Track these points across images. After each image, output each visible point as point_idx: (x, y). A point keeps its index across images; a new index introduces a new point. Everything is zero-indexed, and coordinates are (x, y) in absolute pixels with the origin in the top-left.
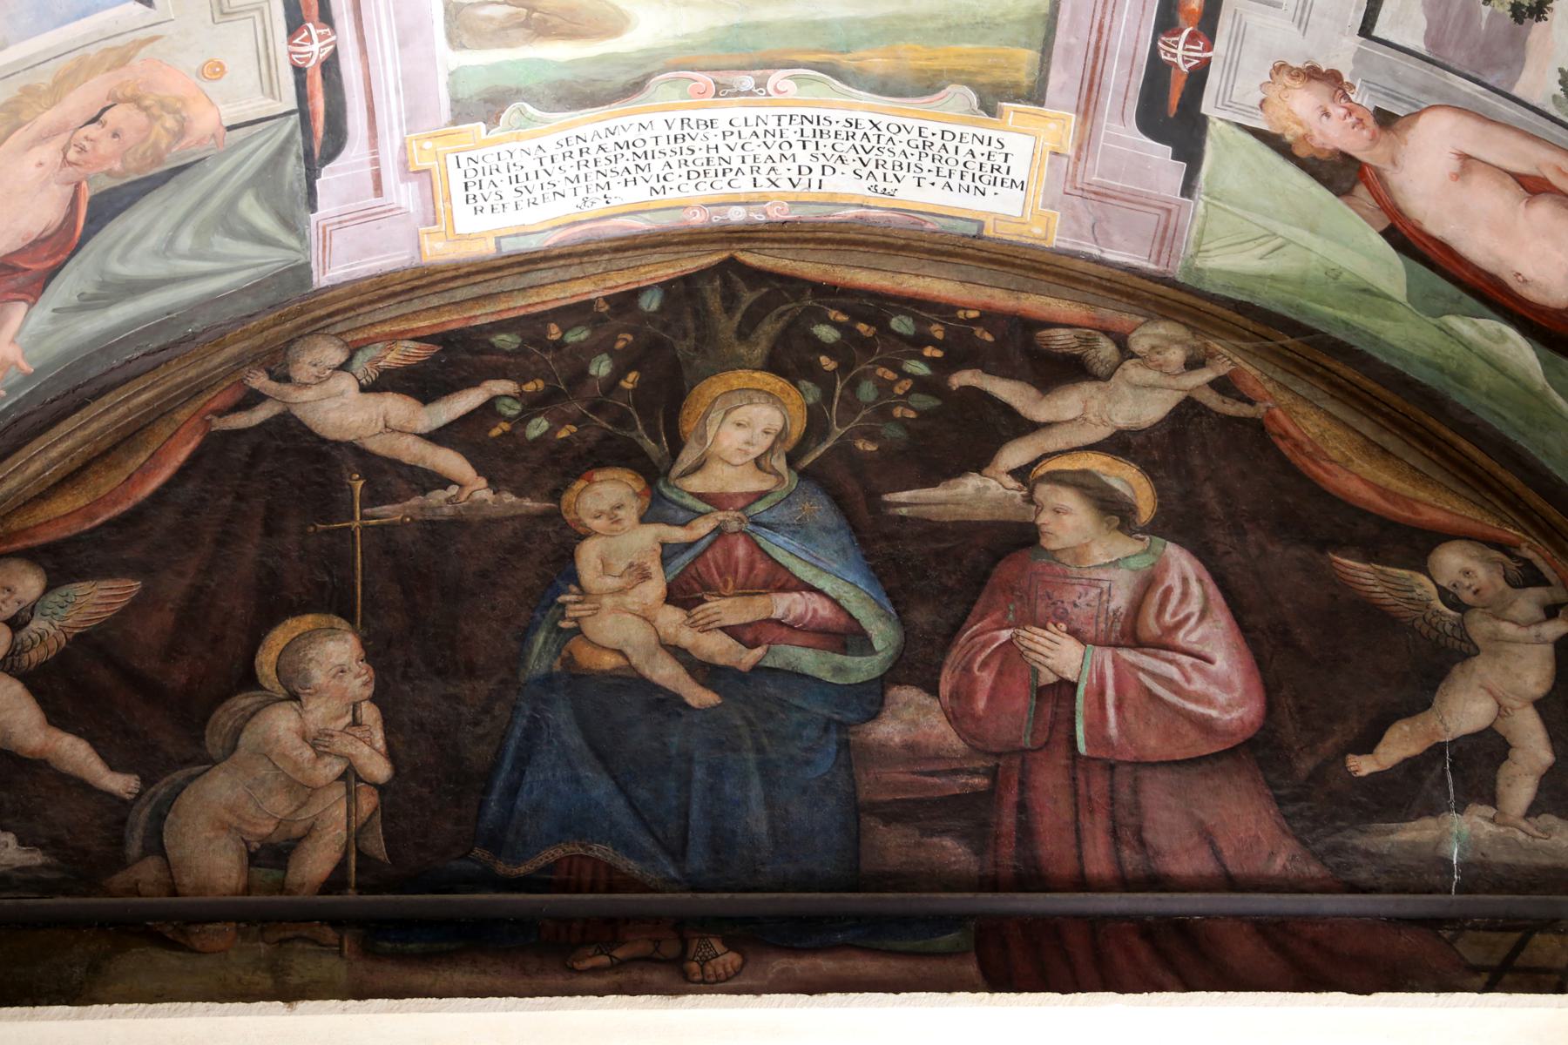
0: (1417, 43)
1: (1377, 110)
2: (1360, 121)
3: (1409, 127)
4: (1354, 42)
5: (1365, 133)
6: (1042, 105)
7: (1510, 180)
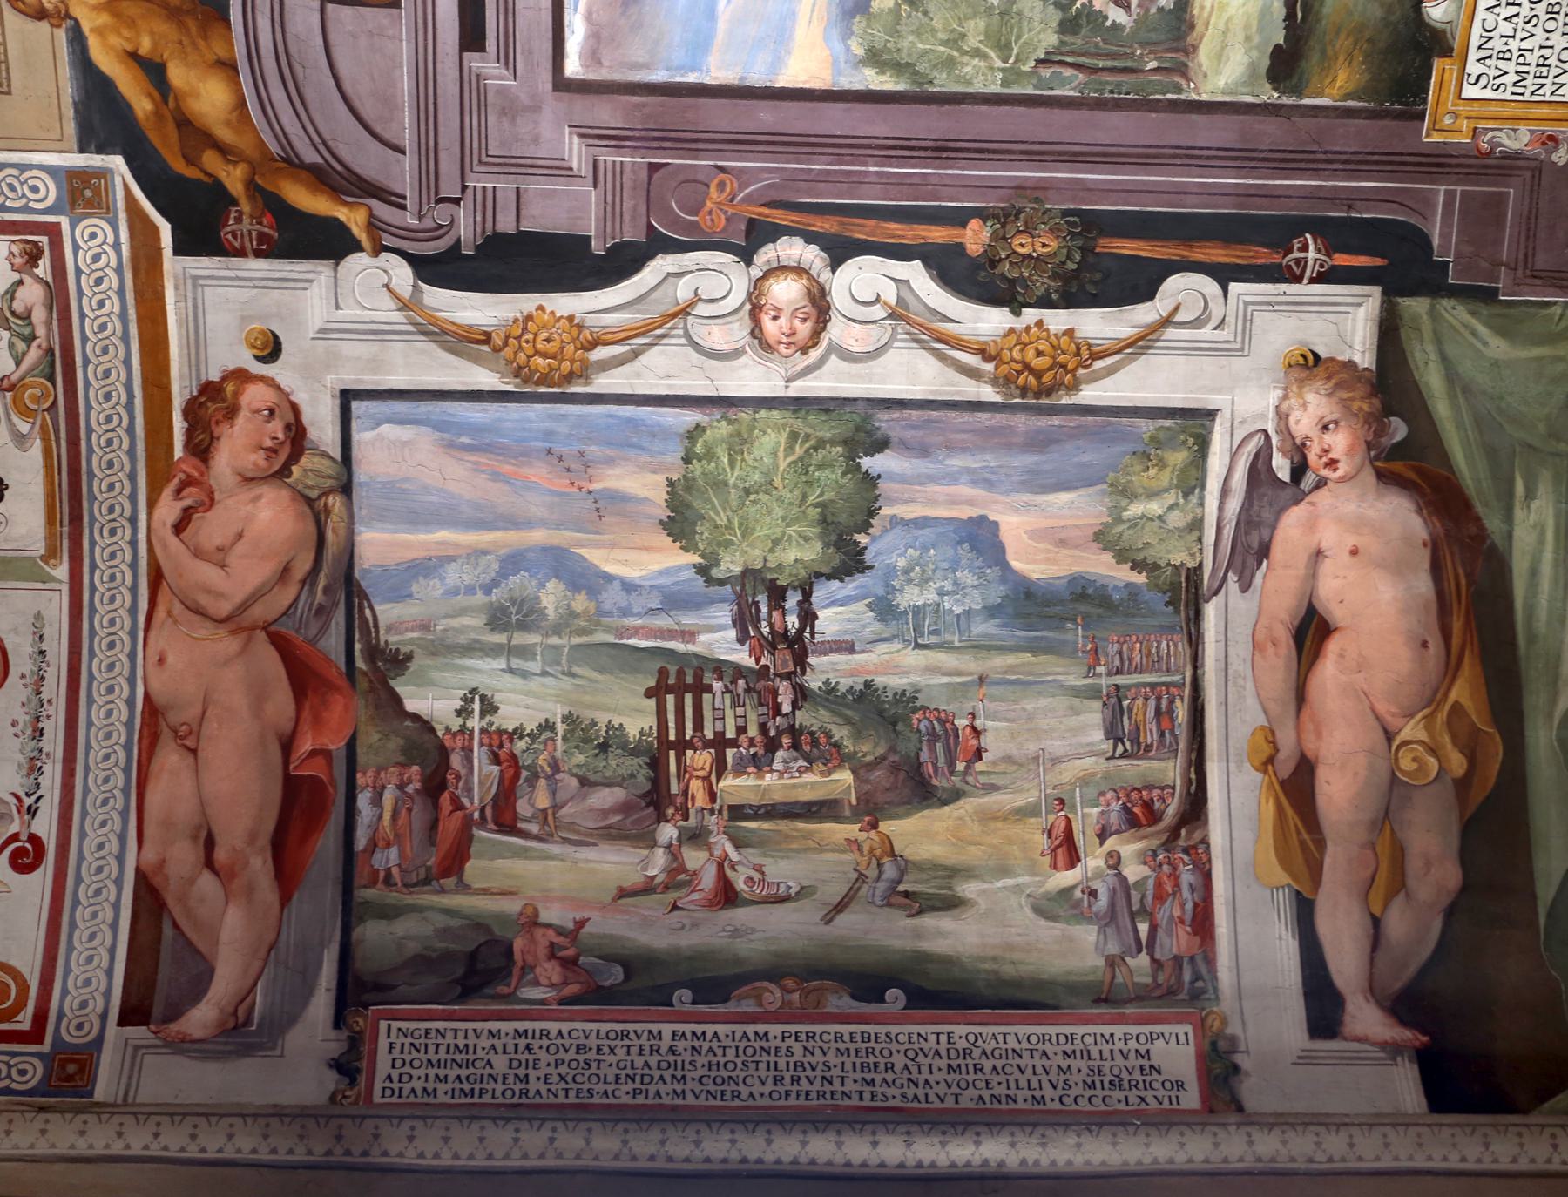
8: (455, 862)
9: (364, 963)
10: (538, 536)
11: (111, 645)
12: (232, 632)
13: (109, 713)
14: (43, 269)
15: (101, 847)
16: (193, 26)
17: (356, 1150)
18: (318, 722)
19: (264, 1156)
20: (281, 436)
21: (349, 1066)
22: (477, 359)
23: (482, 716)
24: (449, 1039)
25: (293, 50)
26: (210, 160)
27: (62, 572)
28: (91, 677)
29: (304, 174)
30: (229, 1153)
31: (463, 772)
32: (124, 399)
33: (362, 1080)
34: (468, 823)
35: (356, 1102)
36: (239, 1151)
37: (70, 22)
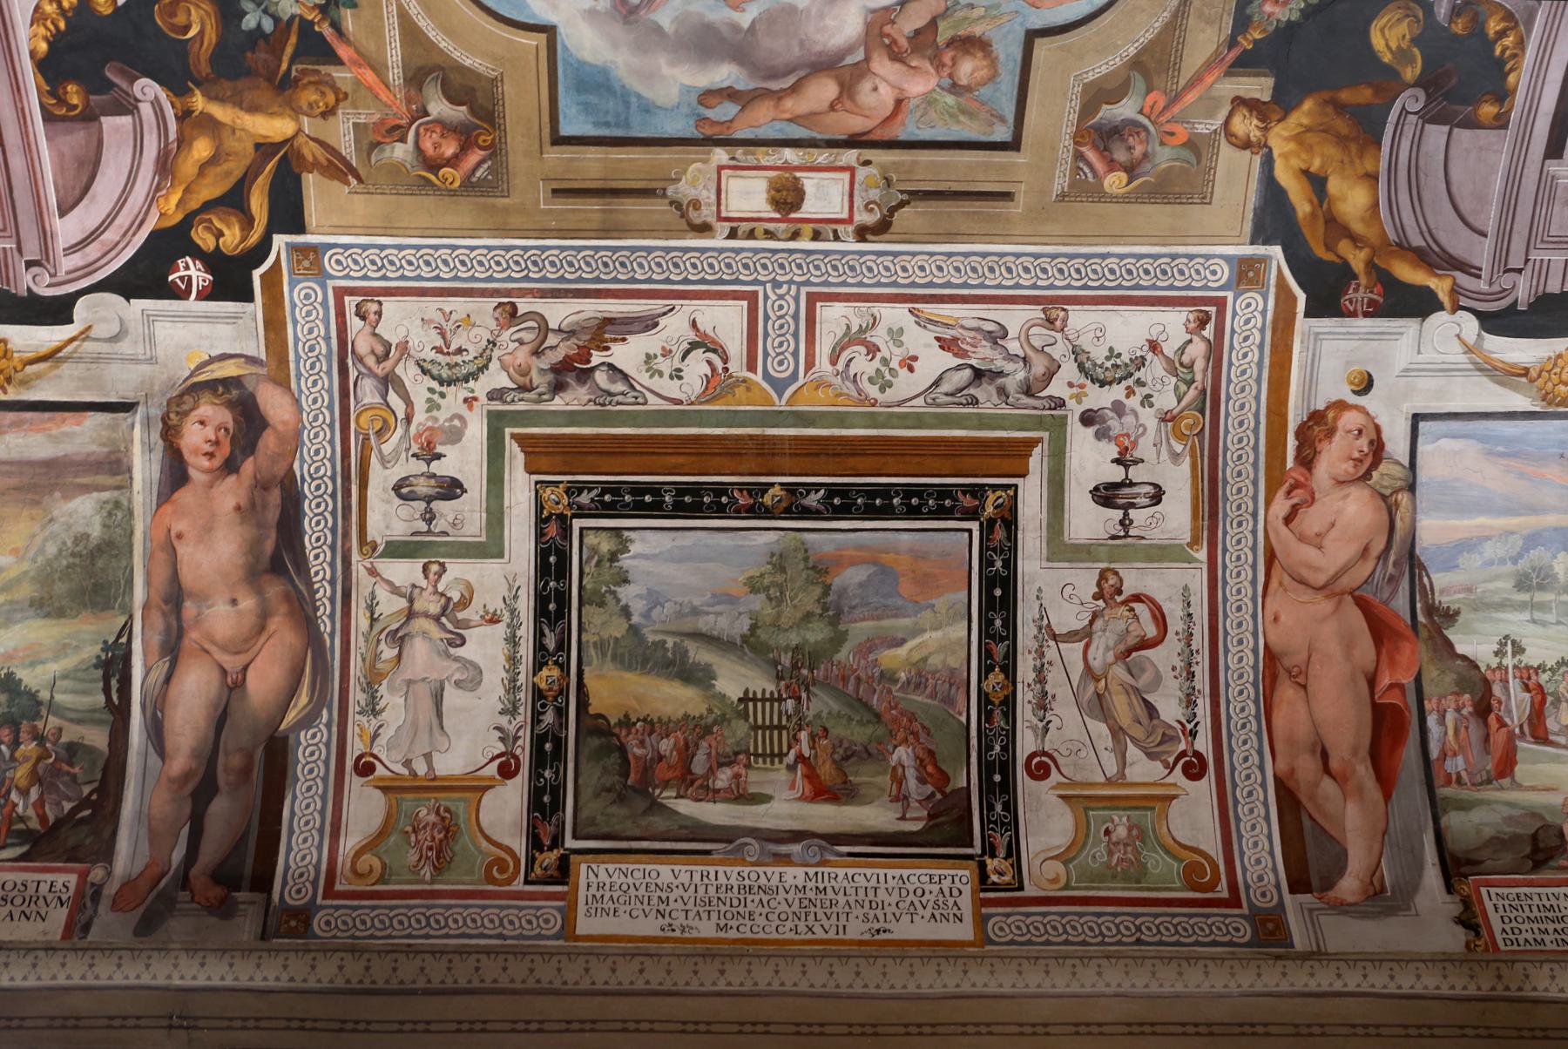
8: (1506, 765)
9: (1455, 844)
10: (1551, 520)
11: (1239, 609)
12: (1327, 597)
13: (1241, 660)
14: (1209, 331)
15: (1246, 759)
16: (1354, 148)
17: (1513, 987)
18: (1393, 663)
19: (1445, 991)
20: (1366, 449)
21: (1470, 919)
22: (1516, 388)
23: (1514, 655)
24: (1536, 901)
25: (1421, 163)
26: (1344, 247)
27: (1202, 555)
28: (1226, 633)
29: (1410, 255)
30: (1419, 990)
31: (1503, 698)
32: (1252, 425)
33: (1484, 932)
34: (1511, 737)
35: (1487, 950)
36: (1426, 988)
37: (1265, 150)
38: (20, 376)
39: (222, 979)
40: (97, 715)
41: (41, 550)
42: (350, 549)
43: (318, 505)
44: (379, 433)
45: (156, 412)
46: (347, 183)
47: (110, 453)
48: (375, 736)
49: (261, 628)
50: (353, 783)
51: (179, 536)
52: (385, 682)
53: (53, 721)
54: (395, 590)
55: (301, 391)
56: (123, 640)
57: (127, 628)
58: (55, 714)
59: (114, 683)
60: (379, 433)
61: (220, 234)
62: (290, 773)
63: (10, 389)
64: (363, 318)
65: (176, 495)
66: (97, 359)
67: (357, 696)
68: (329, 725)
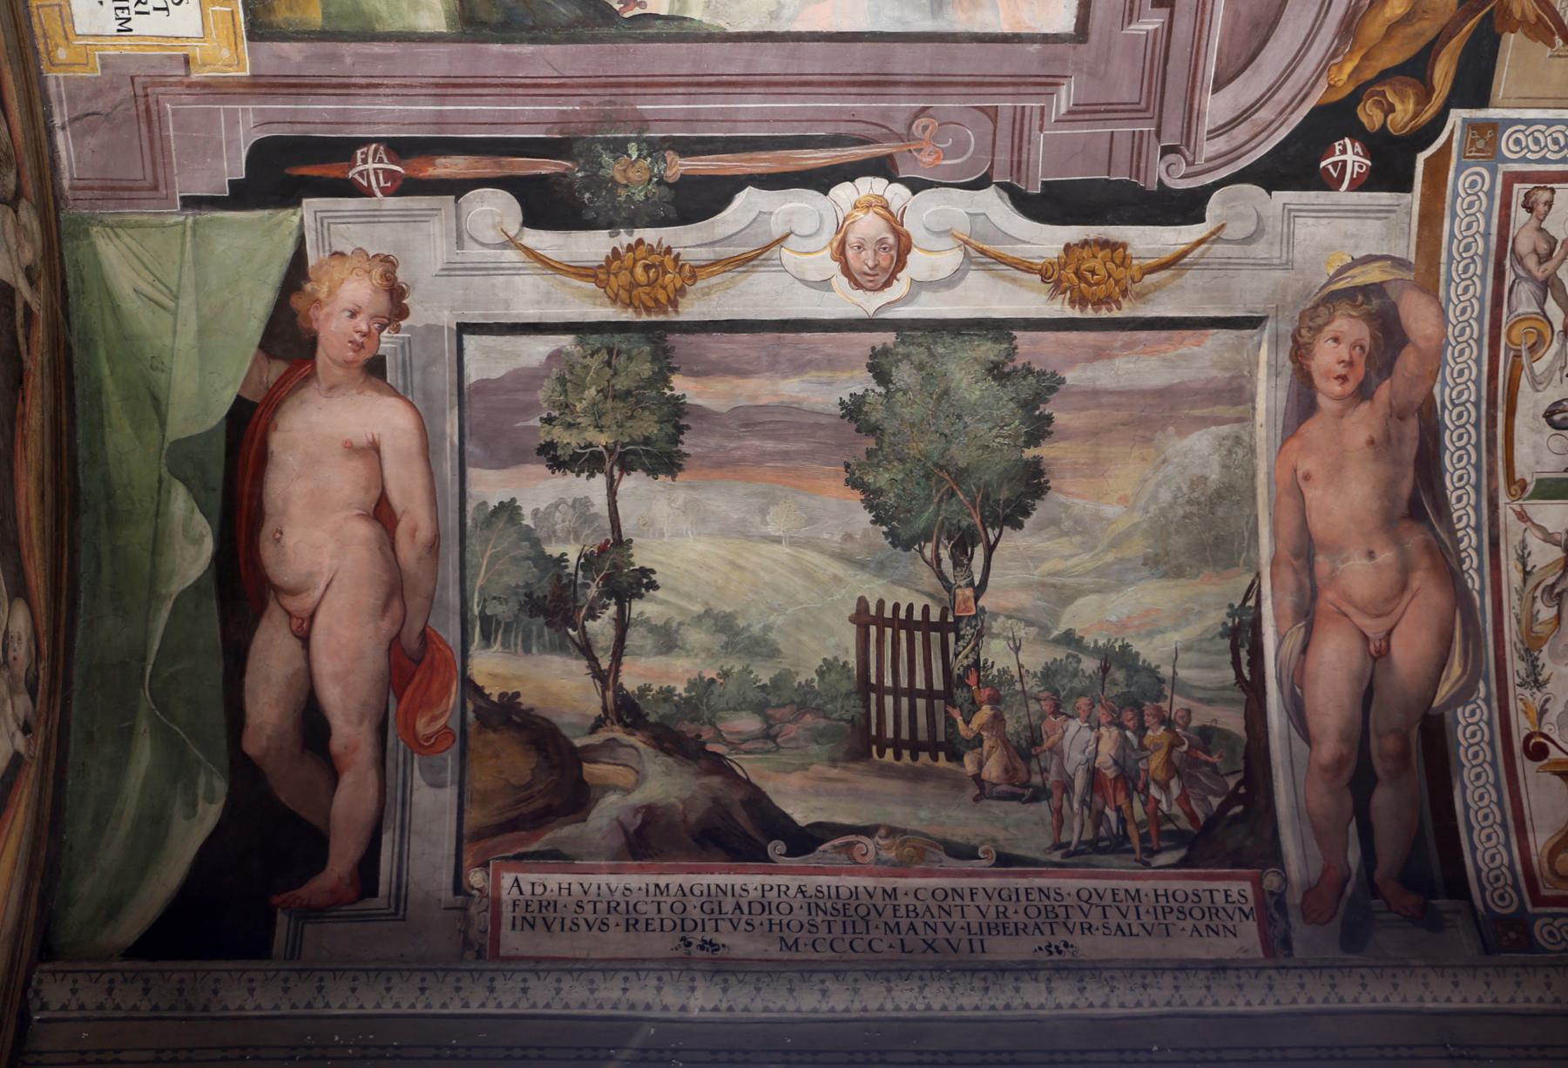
0: (473, 374)
1: (383, 358)
2: (362, 346)
3: (380, 391)
4: (448, 319)
5: (350, 354)
6: (250, 38)
7: (376, 493)
38: (1137, 287)
39: (1480, 1000)
40: (1228, 694)
41: (1154, 498)
42: (1496, 490)
43: (1460, 437)
44: (1532, 349)
45: (1287, 328)
46: (1551, 45)
47: (1233, 378)
48: (1542, 712)
49: (1403, 586)
50: (1527, 769)
51: (1307, 477)
52: (1545, 648)
53: (1180, 702)
54: (1548, 538)
55: (1449, 300)
56: (1251, 603)
57: (1254, 589)
58: (1181, 694)
59: (1244, 655)
60: (1532, 349)
61: (1391, 109)
62: (1452, 758)
63: (1125, 304)
64: (1530, 209)
65: (1304, 427)
66: (1226, 264)
67: (1516, 666)
68: (1487, 700)
